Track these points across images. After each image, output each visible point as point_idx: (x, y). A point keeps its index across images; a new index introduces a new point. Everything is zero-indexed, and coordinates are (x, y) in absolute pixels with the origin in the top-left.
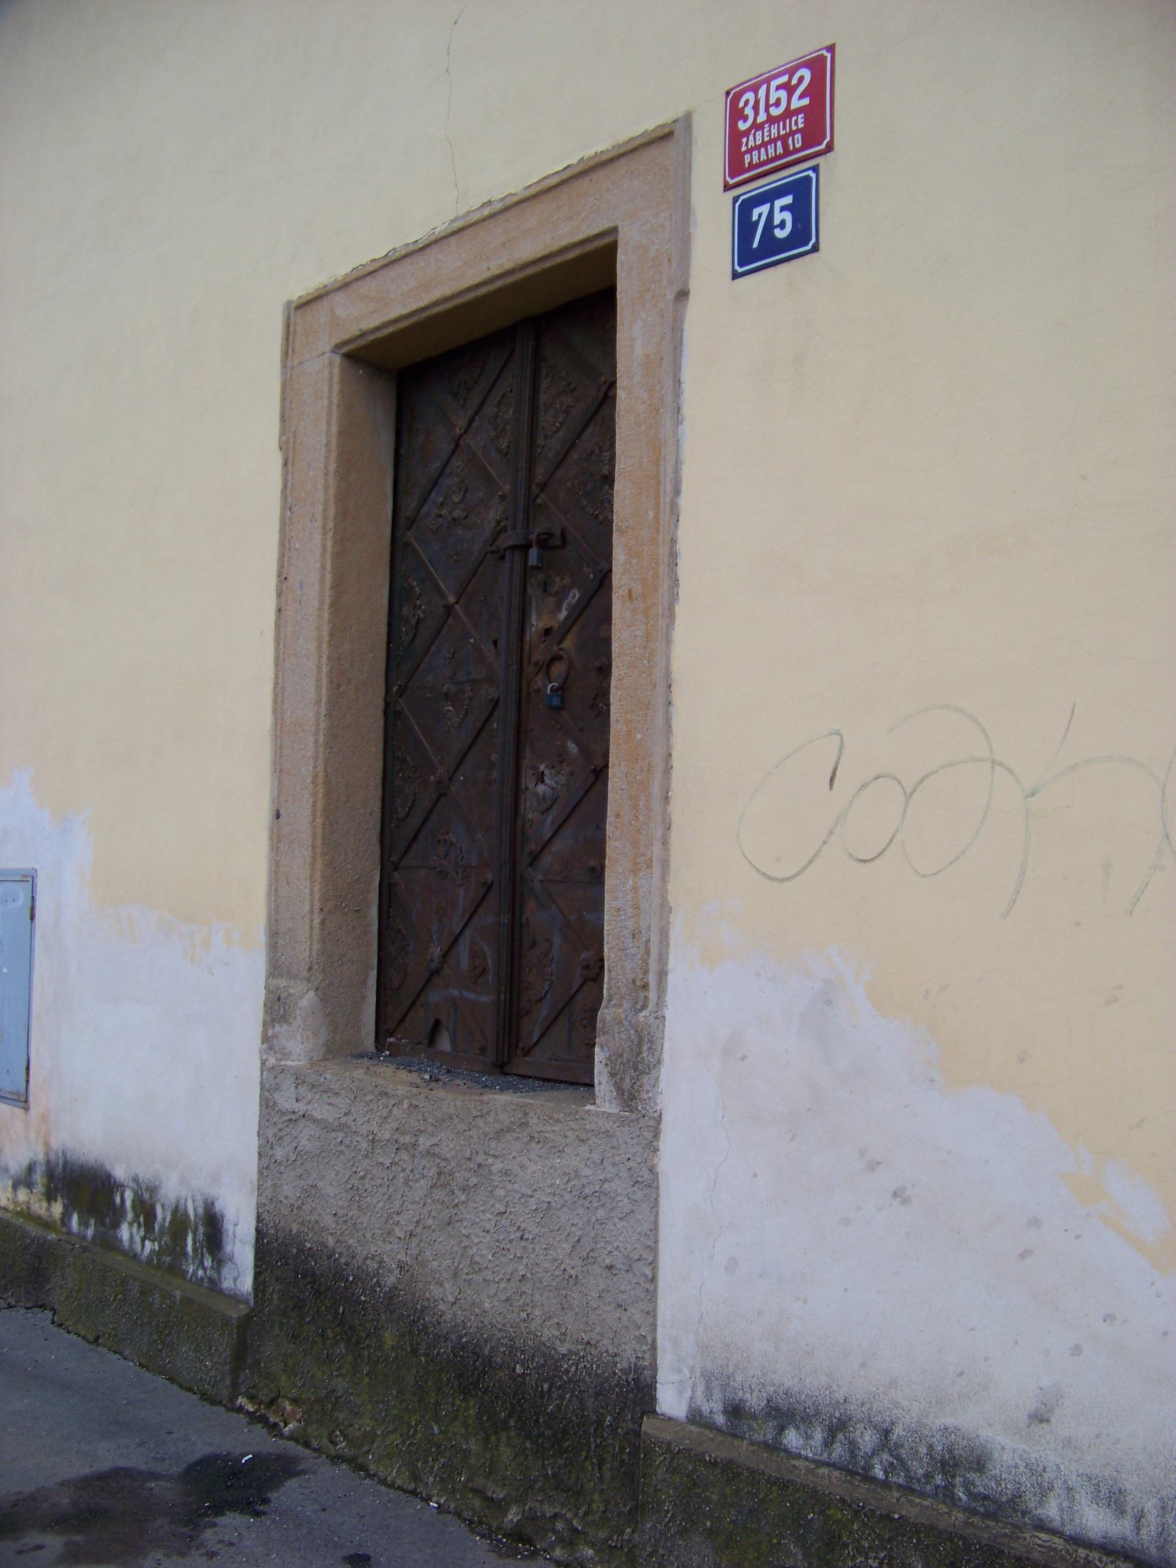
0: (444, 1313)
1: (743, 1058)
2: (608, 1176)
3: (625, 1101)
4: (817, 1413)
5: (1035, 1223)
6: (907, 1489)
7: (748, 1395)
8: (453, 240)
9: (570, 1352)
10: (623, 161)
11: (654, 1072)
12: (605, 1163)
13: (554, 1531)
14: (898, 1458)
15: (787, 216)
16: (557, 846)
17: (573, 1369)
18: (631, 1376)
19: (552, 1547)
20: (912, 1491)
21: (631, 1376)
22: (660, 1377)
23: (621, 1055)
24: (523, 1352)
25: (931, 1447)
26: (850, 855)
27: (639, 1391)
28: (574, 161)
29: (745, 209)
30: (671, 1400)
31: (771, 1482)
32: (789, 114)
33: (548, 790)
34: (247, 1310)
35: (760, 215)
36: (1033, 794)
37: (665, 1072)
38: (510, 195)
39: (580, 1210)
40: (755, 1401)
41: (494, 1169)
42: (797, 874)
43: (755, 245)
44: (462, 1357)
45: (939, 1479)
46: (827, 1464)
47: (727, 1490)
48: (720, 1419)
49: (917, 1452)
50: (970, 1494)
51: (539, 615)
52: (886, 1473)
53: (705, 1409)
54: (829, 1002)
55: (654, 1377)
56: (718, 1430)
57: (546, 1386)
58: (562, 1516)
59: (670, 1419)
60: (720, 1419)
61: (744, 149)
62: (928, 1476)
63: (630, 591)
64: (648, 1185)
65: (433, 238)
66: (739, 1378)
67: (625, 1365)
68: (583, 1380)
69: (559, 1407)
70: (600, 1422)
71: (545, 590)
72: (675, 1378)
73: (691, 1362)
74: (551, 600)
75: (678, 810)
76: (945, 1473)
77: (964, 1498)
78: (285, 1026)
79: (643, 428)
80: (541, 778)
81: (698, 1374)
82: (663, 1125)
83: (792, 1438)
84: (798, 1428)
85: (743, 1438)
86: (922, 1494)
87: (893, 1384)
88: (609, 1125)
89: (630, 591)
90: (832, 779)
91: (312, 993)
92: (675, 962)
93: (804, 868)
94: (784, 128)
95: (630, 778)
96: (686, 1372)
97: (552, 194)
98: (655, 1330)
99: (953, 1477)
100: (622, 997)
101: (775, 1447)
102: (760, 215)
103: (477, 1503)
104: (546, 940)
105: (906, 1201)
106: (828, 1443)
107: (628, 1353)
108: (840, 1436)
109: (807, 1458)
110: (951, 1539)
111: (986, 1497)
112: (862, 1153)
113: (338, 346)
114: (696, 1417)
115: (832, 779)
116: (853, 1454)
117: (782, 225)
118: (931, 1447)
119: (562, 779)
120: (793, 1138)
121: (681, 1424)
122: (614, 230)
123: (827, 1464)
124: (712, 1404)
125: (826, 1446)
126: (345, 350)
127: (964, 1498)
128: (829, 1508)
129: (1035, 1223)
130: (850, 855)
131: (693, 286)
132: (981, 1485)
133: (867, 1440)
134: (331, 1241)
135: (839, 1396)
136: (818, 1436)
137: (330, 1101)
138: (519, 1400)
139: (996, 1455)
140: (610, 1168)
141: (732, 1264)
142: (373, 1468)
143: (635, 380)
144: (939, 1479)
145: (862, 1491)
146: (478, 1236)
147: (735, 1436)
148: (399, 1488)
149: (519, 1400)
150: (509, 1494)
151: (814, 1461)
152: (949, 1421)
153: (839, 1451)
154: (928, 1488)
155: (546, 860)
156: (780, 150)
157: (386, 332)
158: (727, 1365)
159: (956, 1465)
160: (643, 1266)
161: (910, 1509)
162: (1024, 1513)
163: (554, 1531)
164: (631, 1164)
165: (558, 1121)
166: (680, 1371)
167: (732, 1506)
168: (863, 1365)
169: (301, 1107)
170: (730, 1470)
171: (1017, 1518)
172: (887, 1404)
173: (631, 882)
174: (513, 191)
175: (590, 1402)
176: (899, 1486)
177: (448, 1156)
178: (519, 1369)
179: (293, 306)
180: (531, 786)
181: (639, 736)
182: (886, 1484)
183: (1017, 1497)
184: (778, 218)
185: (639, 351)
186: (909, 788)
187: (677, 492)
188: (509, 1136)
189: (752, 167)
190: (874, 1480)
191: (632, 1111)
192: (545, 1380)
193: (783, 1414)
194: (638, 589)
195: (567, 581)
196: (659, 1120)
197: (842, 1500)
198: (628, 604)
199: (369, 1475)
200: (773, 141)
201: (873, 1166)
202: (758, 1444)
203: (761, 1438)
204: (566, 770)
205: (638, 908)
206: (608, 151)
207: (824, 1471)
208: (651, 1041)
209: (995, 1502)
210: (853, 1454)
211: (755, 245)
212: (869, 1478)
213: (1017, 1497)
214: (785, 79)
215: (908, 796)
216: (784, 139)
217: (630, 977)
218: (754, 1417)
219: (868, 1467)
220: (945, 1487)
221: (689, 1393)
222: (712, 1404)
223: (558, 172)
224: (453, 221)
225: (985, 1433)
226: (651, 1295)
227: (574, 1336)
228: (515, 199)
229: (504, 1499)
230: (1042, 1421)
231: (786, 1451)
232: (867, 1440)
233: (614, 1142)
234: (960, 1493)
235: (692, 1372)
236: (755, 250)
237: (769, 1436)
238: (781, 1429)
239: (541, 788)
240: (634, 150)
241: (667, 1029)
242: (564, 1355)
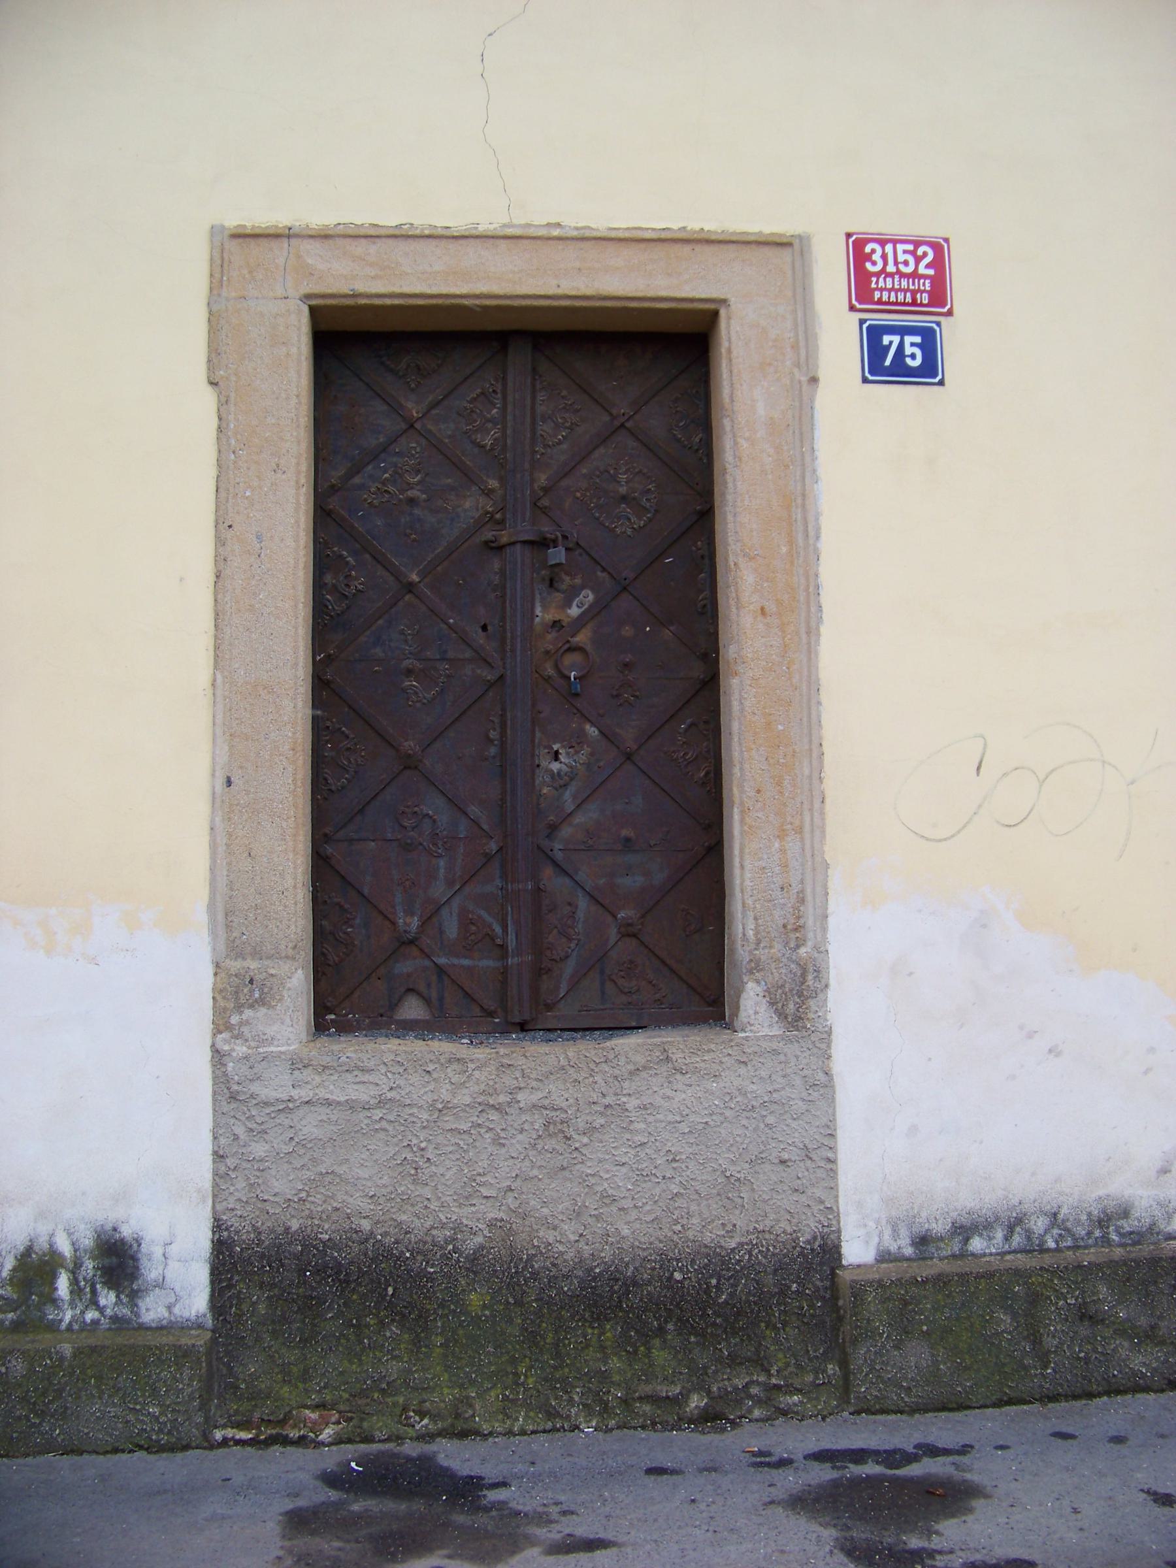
0: (562, 1253)
1: (911, 974)
2: (777, 1086)
3: (789, 1023)
4: (997, 1219)
5: (1152, 1050)
6: (1076, 1247)
7: (934, 1225)
8: (503, 244)
9: (741, 1244)
10: (732, 247)
11: (821, 996)
12: (774, 1077)
13: (750, 1397)
14: (1067, 1230)
15: (918, 352)
16: (579, 819)
17: (747, 1257)
18: (817, 1243)
19: (750, 1411)
20: (1078, 1247)
21: (817, 1243)
22: (845, 1236)
23: (783, 986)
24: (678, 1260)
25: (1089, 1214)
26: (998, 822)
27: (827, 1251)
28: (675, 226)
29: (874, 334)
30: (857, 1250)
31: (979, 1276)
32: (915, 275)
33: (564, 767)
34: (209, 1335)
35: (891, 343)
36: (1132, 783)
37: (831, 994)
38: (589, 228)
39: (744, 1122)
40: (940, 1227)
41: (629, 1106)
42: (953, 836)
43: (888, 363)
44: (594, 1288)
45: (1097, 1233)
46: (1009, 1253)
47: (940, 1297)
48: (909, 1251)
49: (1080, 1220)
50: (1121, 1235)
51: (545, 608)
52: (1057, 1242)
53: (893, 1248)
54: (984, 926)
55: (839, 1238)
56: (908, 1259)
57: (714, 1282)
58: (752, 1382)
59: (859, 1266)
60: (909, 1251)
61: (873, 286)
62: (1089, 1233)
63: (762, 609)
64: (822, 1086)
65: (474, 232)
66: (924, 1214)
67: (808, 1237)
68: (760, 1263)
69: (732, 1295)
70: (783, 1291)
71: (551, 585)
72: (861, 1232)
73: (877, 1216)
74: (559, 596)
75: (832, 784)
76: (1101, 1227)
77: (1116, 1238)
78: (263, 1010)
79: (770, 477)
80: (556, 756)
81: (884, 1222)
82: (833, 1037)
83: (977, 1244)
84: (981, 1235)
85: (932, 1258)
86: (1086, 1247)
87: (1058, 1180)
88: (775, 1045)
89: (762, 609)
90: (978, 769)
91: (300, 971)
92: (834, 905)
93: (959, 832)
94: (913, 284)
95: (771, 761)
96: (872, 1224)
97: (643, 246)
98: (837, 1201)
99: (1108, 1228)
100: (772, 940)
101: (963, 1255)
102: (891, 343)
103: (647, 1408)
104: (570, 904)
105: (1058, 1054)
106: (1007, 1238)
107: (809, 1227)
108: (1018, 1229)
109: (991, 1254)
110: (1125, 1264)
111: (1131, 1233)
112: (1021, 1028)
113: (308, 297)
114: (884, 1257)
115: (978, 769)
116: (1029, 1238)
117: (913, 356)
118: (1089, 1214)
119: (583, 756)
120: (961, 1026)
121: (872, 1266)
122: (724, 301)
123: (1009, 1253)
124: (899, 1242)
125: (1007, 1240)
126: (314, 302)
127: (1116, 1238)
128: (1030, 1277)
129: (1152, 1050)
130: (998, 822)
131: (822, 374)
132: (1127, 1225)
133: (1039, 1225)
134: (366, 1225)
135: (1015, 1201)
136: (999, 1235)
137: (358, 1080)
138: (678, 1304)
139: (1137, 1203)
140: (780, 1080)
141: (913, 1129)
142: (486, 1428)
143: (758, 435)
144: (1097, 1233)
145: (1047, 1260)
146: (608, 1171)
147: (924, 1259)
148: (533, 1432)
149: (678, 1304)
150: (683, 1387)
151: (997, 1254)
152: (1102, 1192)
153: (1017, 1240)
154: (1090, 1241)
155: (566, 832)
156: (909, 299)
157: (388, 302)
158: (912, 1208)
159: (1109, 1219)
160: (821, 1156)
161: (1088, 1257)
162: (1158, 1234)
163: (750, 1397)
164: (805, 1072)
165: (710, 1051)
166: (865, 1226)
167: (944, 1307)
168: (1033, 1174)
169: (305, 1093)
170: (941, 1281)
171: (1154, 1238)
172: (1054, 1195)
173: (777, 845)
174: (593, 226)
175: (769, 1280)
176: (1069, 1248)
177: (564, 1105)
178: (678, 1276)
179: (227, 233)
180: (544, 764)
181: (780, 727)
182: (1058, 1250)
183: (1153, 1224)
184: (908, 350)
185: (761, 410)
186: (1042, 777)
187: (818, 537)
188: (644, 1074)
189: (880, 302)
190: (1048, 1250)
191: (798, 1030)
192: (711, 1277)
193: (964, 1230)
194: (771, 607)
195: (578, 581)
196: (829, 1033)
197: (1041, 1268)
198: (760, 618)
199: (485, 1437)
200: (905, 291)
201: (1030, 1035)
202: (947, 1258)
203: (949, 1253)
204: (586, 750)
205: (786, 866)
206: (716, 232)
207: (1008, 1257)
208: (817, 971)
209: (1138, 1233)
210: (1029, 1238)
211: (888, 363)
212: (1043, 1250)
213: (1153, 1224)
214: (910, 247)
215: (1042, 783)
216: (914, 293)
217: (781, 922)
218: (941, 1239)
219: (1042, 1242)
220: (1103, 1237)
221: (876, 1240)
222: (899, 1242)
223: (653, 230)
224: (504, 226)
225: (1128, 1192)
226: (833, 1173)
227: (745, 1229)
228: (595, 234)
229: (680, 1393)
230: (1166, 1173)
231: (973, 1254)
232: (1039, 1225)
233: (782, 1057)
234: (1114, 1237)
235: (878, 1222)
236: (881, 365)
237: (956, 1249)
238: (966, 1240)
239: (555, 766)
240: (747, 243)
241: (831, 960)
242: (733, 1250)
